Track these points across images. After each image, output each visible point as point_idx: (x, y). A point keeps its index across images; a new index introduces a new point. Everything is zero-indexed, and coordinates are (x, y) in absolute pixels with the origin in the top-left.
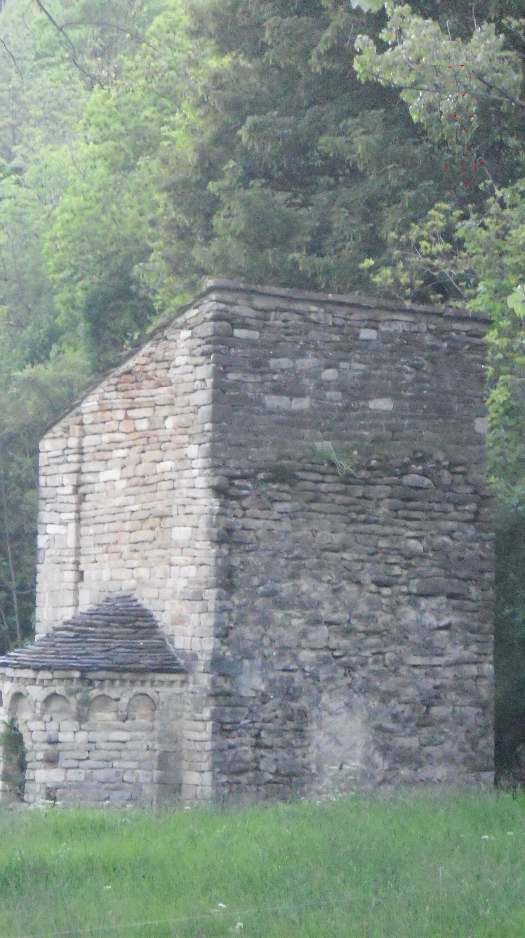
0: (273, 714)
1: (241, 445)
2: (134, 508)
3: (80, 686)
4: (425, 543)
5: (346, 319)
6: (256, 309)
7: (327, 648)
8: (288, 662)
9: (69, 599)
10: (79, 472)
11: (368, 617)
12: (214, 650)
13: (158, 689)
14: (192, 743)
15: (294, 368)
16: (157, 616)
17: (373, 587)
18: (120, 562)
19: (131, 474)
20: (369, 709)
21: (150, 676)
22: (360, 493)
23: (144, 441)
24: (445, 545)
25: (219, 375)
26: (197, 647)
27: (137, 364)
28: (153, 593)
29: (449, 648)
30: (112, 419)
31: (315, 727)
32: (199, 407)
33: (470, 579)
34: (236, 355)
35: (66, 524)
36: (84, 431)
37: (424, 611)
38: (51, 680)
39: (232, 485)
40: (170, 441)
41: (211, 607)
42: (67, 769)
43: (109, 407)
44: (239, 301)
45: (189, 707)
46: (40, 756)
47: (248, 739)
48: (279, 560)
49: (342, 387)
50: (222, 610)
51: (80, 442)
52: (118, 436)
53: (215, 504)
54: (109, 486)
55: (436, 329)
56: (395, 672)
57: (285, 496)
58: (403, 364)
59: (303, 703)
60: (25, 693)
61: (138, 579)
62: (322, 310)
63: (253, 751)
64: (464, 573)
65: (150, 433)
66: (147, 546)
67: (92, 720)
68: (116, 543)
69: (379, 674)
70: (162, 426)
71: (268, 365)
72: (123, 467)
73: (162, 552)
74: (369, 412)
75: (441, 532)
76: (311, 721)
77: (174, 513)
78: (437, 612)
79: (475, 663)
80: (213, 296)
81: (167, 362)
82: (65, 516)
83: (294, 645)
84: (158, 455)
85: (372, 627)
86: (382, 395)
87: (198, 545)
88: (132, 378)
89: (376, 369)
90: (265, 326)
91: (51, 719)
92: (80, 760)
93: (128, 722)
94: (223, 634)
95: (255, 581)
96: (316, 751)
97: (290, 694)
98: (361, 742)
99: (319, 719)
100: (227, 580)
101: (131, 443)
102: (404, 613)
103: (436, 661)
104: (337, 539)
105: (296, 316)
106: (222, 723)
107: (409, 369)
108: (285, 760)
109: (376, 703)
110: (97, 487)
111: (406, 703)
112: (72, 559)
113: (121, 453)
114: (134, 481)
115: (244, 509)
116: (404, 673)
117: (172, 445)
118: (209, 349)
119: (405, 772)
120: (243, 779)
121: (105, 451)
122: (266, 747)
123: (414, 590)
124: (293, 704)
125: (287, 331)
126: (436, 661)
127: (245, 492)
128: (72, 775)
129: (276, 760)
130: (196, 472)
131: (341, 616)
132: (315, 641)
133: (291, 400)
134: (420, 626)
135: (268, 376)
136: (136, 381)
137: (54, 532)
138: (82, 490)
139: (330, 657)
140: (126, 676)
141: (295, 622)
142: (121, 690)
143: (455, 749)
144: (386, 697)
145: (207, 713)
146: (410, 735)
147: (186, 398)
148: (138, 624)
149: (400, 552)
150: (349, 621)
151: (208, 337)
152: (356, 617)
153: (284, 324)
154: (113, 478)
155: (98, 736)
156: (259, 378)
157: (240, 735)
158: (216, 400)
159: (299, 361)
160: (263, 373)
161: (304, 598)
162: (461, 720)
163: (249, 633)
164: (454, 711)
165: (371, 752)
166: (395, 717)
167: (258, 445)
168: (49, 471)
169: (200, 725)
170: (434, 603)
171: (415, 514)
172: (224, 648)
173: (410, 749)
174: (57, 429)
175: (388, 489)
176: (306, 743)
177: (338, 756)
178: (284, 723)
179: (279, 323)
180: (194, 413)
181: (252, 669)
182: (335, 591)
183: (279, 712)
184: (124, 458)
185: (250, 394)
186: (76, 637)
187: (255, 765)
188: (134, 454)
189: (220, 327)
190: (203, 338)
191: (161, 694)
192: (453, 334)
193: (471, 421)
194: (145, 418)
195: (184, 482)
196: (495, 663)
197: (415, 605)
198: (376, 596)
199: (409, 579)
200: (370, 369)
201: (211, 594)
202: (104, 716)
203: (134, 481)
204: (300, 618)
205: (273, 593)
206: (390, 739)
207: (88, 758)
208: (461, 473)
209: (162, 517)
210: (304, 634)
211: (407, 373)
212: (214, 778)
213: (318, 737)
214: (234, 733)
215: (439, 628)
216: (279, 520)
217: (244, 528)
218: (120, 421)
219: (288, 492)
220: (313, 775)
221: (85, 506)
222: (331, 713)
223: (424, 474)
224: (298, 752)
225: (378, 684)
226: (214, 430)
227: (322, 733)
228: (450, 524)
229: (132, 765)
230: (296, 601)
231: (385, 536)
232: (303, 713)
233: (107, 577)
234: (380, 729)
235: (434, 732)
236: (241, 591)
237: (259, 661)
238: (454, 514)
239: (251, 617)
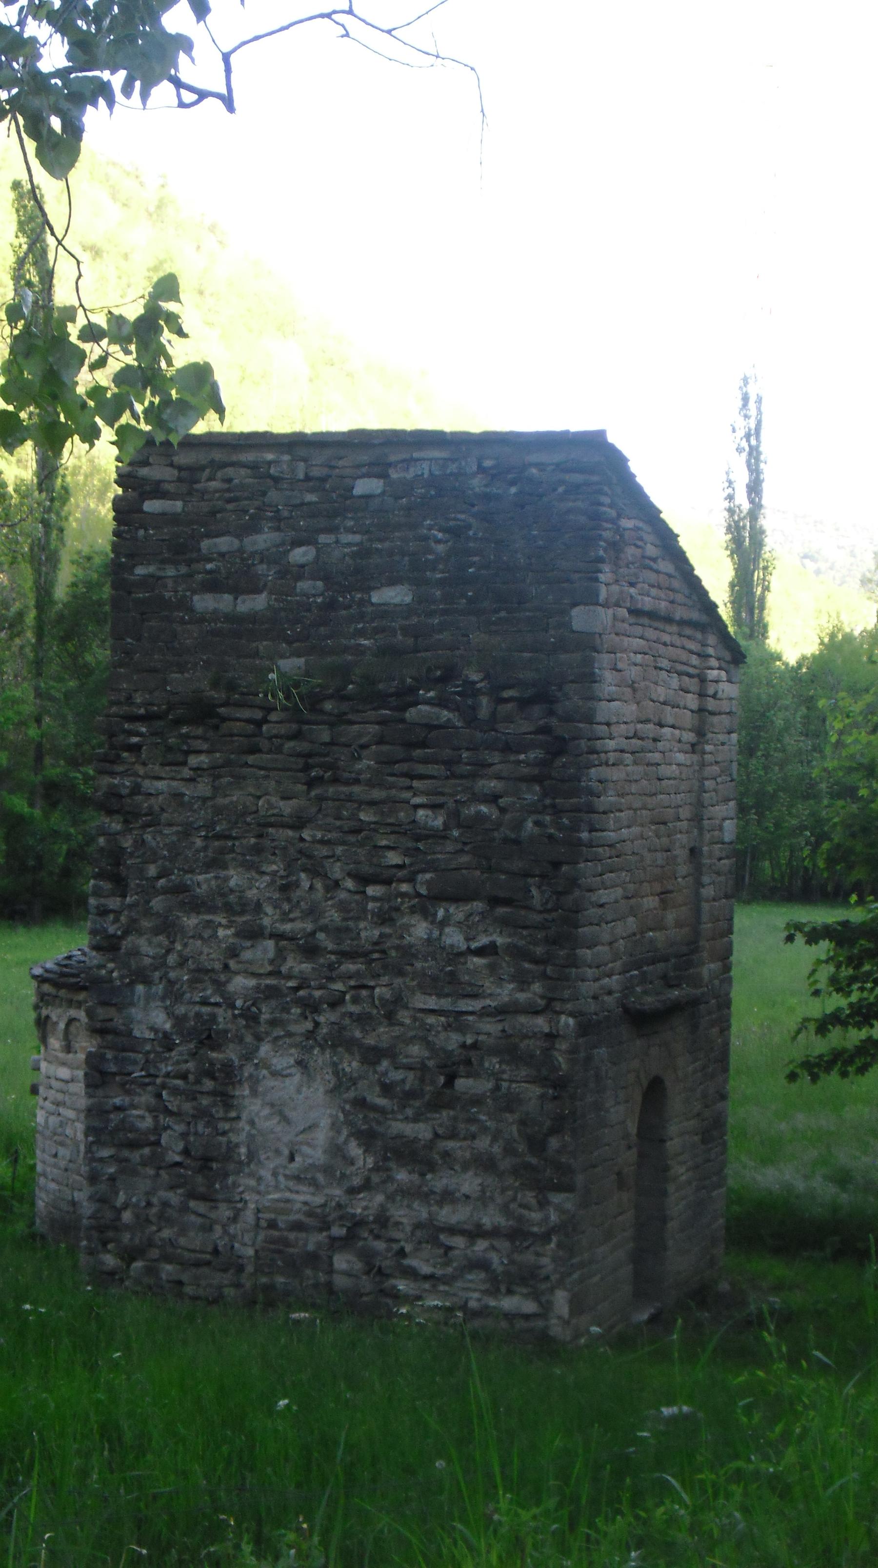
1: (154, 670)
6: (180, 468)
8: (209, 992)
11: (338, 930)
15: (241, 550)
20: (337, 1073)
22: (326, 737)
24: (480, 818)
31: (247, 1092)
47: (145, 1098)
56: (390, 1017)
57: (199, 744)
58: (430, 528)
59: (232, 1053)
62: (286, 458)
64: (517, 865)
69: (362, 1020)
74: (370, 609)
75: (478, 798)
76: (240, 1082)
78: (468, 927)
85: (346, 946)
86: (392, 582)
89: (381, 540)
95: (152, 870)
96: (247, 1128)
97: (207, 1037)
98: (325, 1122)
99: (254, 1081)
102: (407, 927)
103: (465, 1005)
104: (287, 807)
105: (243, 472)
107: (440, 535)
109: (355, 1064)
111: (409, 1068)
116: (408, 1021)
119: (402, 1176)
120: (135, 1156)
123: (423, 891)
125: (227, 495)
126: (465, 1005)
131: (301, 926)
132: (250, 962)
133: (236, 599)
143: (496, 1149)
144: (372, 1056)
146: (416, 1119)
149: (397, 829)
153: (226, 486)
156: (184, 570)
159: (247, 540)
161: (232, 898)
162: (510, 1102)
163: (147, 947)
165: (342, 1138)
167: (182, 668)
170: (458, 912)
171: (421, 769)
173: (416, 1140)
175: (373, 729)
176: (233, 1114)
177: (286, 1139)
181: (149, 998)
185: (167, 595)
187: (152, 1138)
192: (534, 471)
197: (427, 914)
200: (370, 540)
204: (227, 927)
205: (181, 889)
210: (233, 952)
211: (439, 542)
213: (254, 1108)
216: (192, 780)
219: (204, 739)
220: (241, 1163)
222: (275, 1074)
223: (441, 702)
225: (358, 1034)
227: (259, 1102)
228: (493, 784)
231: (372, 803)
234: (361, 1103)
235: (455, 1119)
237: (159, 989)
239: (146, 924)
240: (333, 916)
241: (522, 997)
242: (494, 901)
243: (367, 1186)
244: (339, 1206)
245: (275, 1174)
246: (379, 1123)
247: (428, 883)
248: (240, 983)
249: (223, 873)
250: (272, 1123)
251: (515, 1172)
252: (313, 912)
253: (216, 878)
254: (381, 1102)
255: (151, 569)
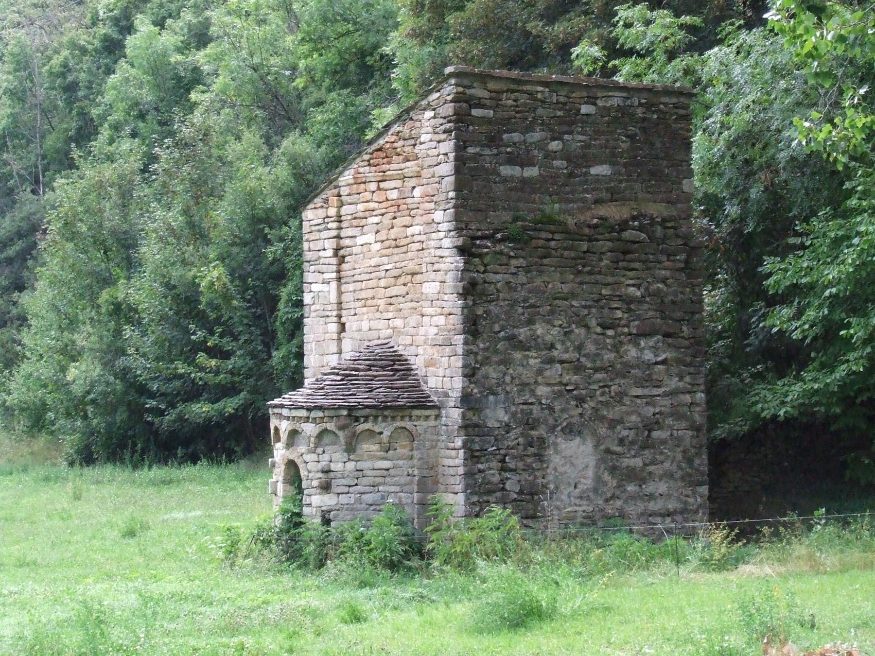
0: (516, 442)
2: (388, 267)
3: (348, 421)
4: (642, 290)
5: (569, 97)
7: (561, 383)
8: (527, 397)
9: (334, 348)
10: (338, 237)
12: (463, 388)
13: (415, 423)
14: (446, 468)
15: (525, 142)
16: (412, 360)
17: (599, 330)
18: (378, 315)
19: (384, 238)
21: (407, 412)
22: (585, 248)
23: (395, 209)
25: (460, 148)
26: (448, 385)
27: (387, 142)
28: (408, 340)
29: (667, 381)
30: (366, 191)
32: (443, 177)
33: (684, 320)
34: (473, 131)
35: (329, 283)
36: (341, 201)
37: (644, 348)
38: (322, 418)
39: (475, 244)
40: (418, 208)
41: (460, 351)
42: (339, 494)
43: (363, 180)
44: (475, 85)
45: (444, 438)
46: (315, 483)
47: (495, 464)
48: (517, 308)
49: (566, 155)
50: (467, 353)
51: (339, 212)
52: (372, 205)
53: (459, 262)
54: (365, 248)
55: (646, 103)
59: (542, 431)
60: (300, 430)
61: (394, 328)
62: (547, 90)
63: (500, 474)
64: (678, 315)
65: (400, 201)
66: (401, 299)
67: (359, 452)
68: (373, 298)
69: (606, 404)
70: (410, 195)
71: (502, 140)
72: (377, 232)
73: (414, 304)
77: (424, 270)
78: (655, 349)
79: (689, 392)
80: (453, 81)
81: (415, 140)
82: (327, 276)
83: (532, 381)
84: (407, 220)
85: (598, 364)
86: (602, 163)
87: (446, 297)
88: (383, 155)
89: (595, 140)
90: (497, 106)
91: (324, 452)
92: (350, 486)
93: (391, 452)
94: (470, 373)
95: (497, 328)
97: (530, 424)
100: (472, 327)
101: (384, 211)
103: (656, 391)
104: (566, 288)
105: (526, 96)
106: (472, 451)
108: (526, 480)
110: (355, 250)
112: (335, 313)
113: (376, 220)
114: (387, 243)
115: (485, 266)
117: (420, 212)
118: (451, 127)
119: (631, 488)
121: (360, 218)
122: (511, 470)
123: (635, 331)
124: (533, 432)
126: (656, 391)
127: (486, 250)
128: (343, 499)
129: (519, 481)
130: (442, 235)
131: (572, 355)
134: (641, 364)
135: (503, 149)
136: (387, 157)
137: (318, 290)
138: (341, 252)
139: (563, 391)
140: (386, 413)
141: (532, 362)
142: (383, 425)
143: (674, 468)
144: (613, 424)
145: (459, 442)
146: (634, 457)
147: (431, 170)
148: (396, 367)
150: (579, 359)
151: (449, 116)
152: (584, 356)
154: (369, 242)
155: (365, 465)
157: (487, 461)
158: (458, 171)
160: (497, 147)
163: (492, 372)
164: (672, 435)
166: (621, 442)
168: (312, 237)
169: (453, 453)
170: (652, 342)
172: (472, 386)
173: (634, 469)
174: (318, 201)
175: (609, 244)
178: (525, 449)
179: (510, 102)
180: (439, 183)
181: (496, 403)
182: (566, 333)
183: (521, 440)
184: (377, 224)
186: (342, 380)
188: (386, 220)
189: (460, 107)
190: (445, 118)
191: (418, 427)
192: (662, 106)
193: (680, 183)
194: (395, 188)
195: (432, 243)
196: (707, 392)
198: (601, 337)
199: (630, 321)
201: (459, 339)
202: (369, 447)
203: (387, 243)
204: (536, 358)
205: (511, 338)
206: (617, 461)
207: (356, 485)
208: (672, 227)
209: (413, 274)
210: (540, 372)
212: (467, 498)
213: (555, 460)
214: (483, 459)
215: (657, 363)
217: (485, 282)
218: (374, 192)
221: (345, 266)
223: (641, 229)
224: (538, 474)
226: (457, 198)
227: (558, 457)
229: (393, 489)
230: (533, 343)
232: (542, 440)
233: (368, 328)
234: (608, 451)
235: (655, 453)
236: (485, 336)
237: (502, 397)
238: (667, 264)
239: (495, 359)
240: (590, 348)
241: (681, 384)
242: (667, 335)
243: (613, 497)
244: (601, 510)
245: (569, 497)
246: (617, 461)
247: (638, 327)
248: (542, 390)
249: (533, 327)
250: (567, 468)
251: (683, 479)
252: (579, 348)
253: (530, 330)
254: (618, 449)
255: (478, 149)
